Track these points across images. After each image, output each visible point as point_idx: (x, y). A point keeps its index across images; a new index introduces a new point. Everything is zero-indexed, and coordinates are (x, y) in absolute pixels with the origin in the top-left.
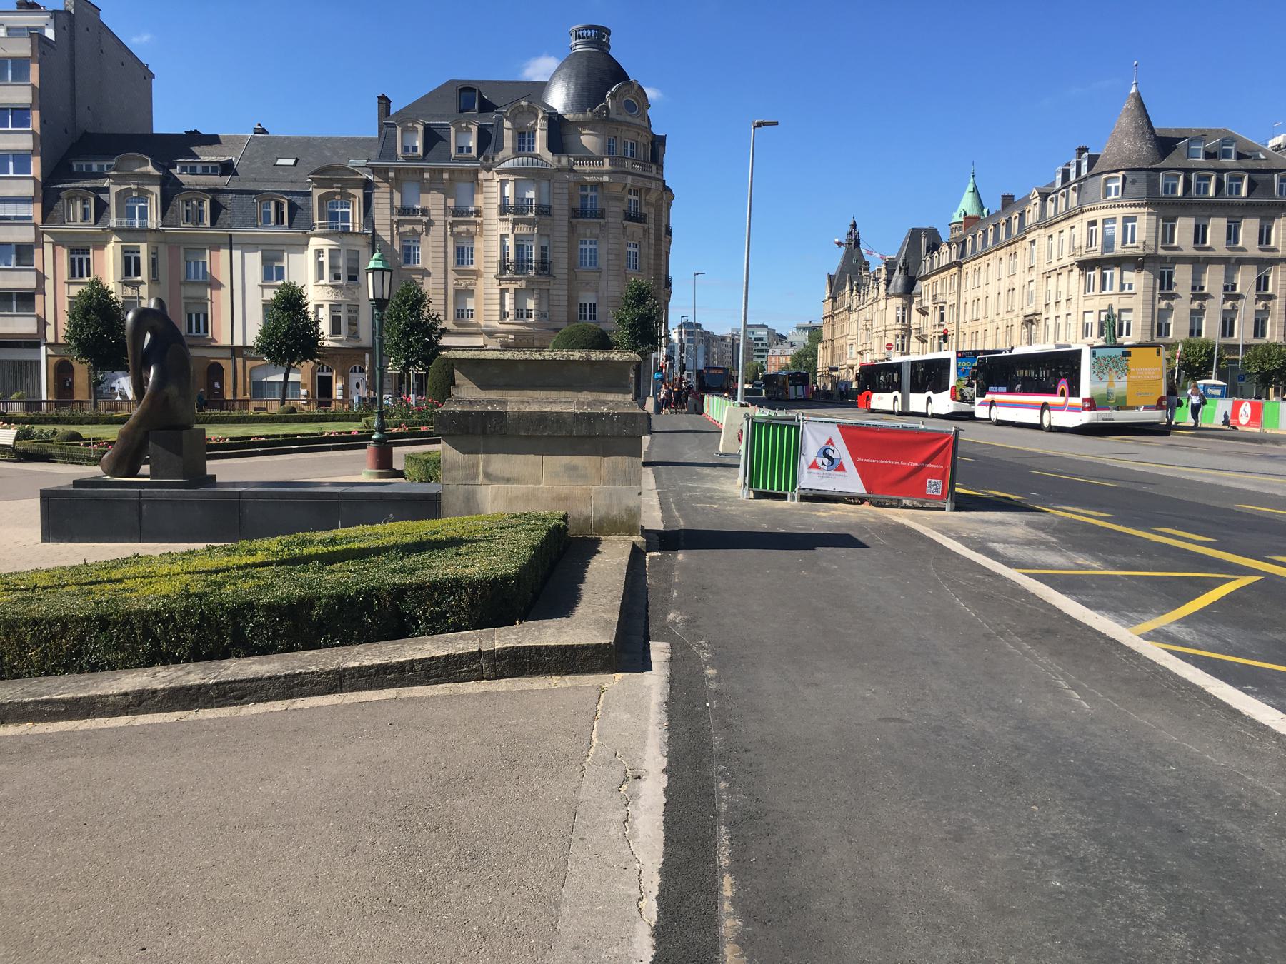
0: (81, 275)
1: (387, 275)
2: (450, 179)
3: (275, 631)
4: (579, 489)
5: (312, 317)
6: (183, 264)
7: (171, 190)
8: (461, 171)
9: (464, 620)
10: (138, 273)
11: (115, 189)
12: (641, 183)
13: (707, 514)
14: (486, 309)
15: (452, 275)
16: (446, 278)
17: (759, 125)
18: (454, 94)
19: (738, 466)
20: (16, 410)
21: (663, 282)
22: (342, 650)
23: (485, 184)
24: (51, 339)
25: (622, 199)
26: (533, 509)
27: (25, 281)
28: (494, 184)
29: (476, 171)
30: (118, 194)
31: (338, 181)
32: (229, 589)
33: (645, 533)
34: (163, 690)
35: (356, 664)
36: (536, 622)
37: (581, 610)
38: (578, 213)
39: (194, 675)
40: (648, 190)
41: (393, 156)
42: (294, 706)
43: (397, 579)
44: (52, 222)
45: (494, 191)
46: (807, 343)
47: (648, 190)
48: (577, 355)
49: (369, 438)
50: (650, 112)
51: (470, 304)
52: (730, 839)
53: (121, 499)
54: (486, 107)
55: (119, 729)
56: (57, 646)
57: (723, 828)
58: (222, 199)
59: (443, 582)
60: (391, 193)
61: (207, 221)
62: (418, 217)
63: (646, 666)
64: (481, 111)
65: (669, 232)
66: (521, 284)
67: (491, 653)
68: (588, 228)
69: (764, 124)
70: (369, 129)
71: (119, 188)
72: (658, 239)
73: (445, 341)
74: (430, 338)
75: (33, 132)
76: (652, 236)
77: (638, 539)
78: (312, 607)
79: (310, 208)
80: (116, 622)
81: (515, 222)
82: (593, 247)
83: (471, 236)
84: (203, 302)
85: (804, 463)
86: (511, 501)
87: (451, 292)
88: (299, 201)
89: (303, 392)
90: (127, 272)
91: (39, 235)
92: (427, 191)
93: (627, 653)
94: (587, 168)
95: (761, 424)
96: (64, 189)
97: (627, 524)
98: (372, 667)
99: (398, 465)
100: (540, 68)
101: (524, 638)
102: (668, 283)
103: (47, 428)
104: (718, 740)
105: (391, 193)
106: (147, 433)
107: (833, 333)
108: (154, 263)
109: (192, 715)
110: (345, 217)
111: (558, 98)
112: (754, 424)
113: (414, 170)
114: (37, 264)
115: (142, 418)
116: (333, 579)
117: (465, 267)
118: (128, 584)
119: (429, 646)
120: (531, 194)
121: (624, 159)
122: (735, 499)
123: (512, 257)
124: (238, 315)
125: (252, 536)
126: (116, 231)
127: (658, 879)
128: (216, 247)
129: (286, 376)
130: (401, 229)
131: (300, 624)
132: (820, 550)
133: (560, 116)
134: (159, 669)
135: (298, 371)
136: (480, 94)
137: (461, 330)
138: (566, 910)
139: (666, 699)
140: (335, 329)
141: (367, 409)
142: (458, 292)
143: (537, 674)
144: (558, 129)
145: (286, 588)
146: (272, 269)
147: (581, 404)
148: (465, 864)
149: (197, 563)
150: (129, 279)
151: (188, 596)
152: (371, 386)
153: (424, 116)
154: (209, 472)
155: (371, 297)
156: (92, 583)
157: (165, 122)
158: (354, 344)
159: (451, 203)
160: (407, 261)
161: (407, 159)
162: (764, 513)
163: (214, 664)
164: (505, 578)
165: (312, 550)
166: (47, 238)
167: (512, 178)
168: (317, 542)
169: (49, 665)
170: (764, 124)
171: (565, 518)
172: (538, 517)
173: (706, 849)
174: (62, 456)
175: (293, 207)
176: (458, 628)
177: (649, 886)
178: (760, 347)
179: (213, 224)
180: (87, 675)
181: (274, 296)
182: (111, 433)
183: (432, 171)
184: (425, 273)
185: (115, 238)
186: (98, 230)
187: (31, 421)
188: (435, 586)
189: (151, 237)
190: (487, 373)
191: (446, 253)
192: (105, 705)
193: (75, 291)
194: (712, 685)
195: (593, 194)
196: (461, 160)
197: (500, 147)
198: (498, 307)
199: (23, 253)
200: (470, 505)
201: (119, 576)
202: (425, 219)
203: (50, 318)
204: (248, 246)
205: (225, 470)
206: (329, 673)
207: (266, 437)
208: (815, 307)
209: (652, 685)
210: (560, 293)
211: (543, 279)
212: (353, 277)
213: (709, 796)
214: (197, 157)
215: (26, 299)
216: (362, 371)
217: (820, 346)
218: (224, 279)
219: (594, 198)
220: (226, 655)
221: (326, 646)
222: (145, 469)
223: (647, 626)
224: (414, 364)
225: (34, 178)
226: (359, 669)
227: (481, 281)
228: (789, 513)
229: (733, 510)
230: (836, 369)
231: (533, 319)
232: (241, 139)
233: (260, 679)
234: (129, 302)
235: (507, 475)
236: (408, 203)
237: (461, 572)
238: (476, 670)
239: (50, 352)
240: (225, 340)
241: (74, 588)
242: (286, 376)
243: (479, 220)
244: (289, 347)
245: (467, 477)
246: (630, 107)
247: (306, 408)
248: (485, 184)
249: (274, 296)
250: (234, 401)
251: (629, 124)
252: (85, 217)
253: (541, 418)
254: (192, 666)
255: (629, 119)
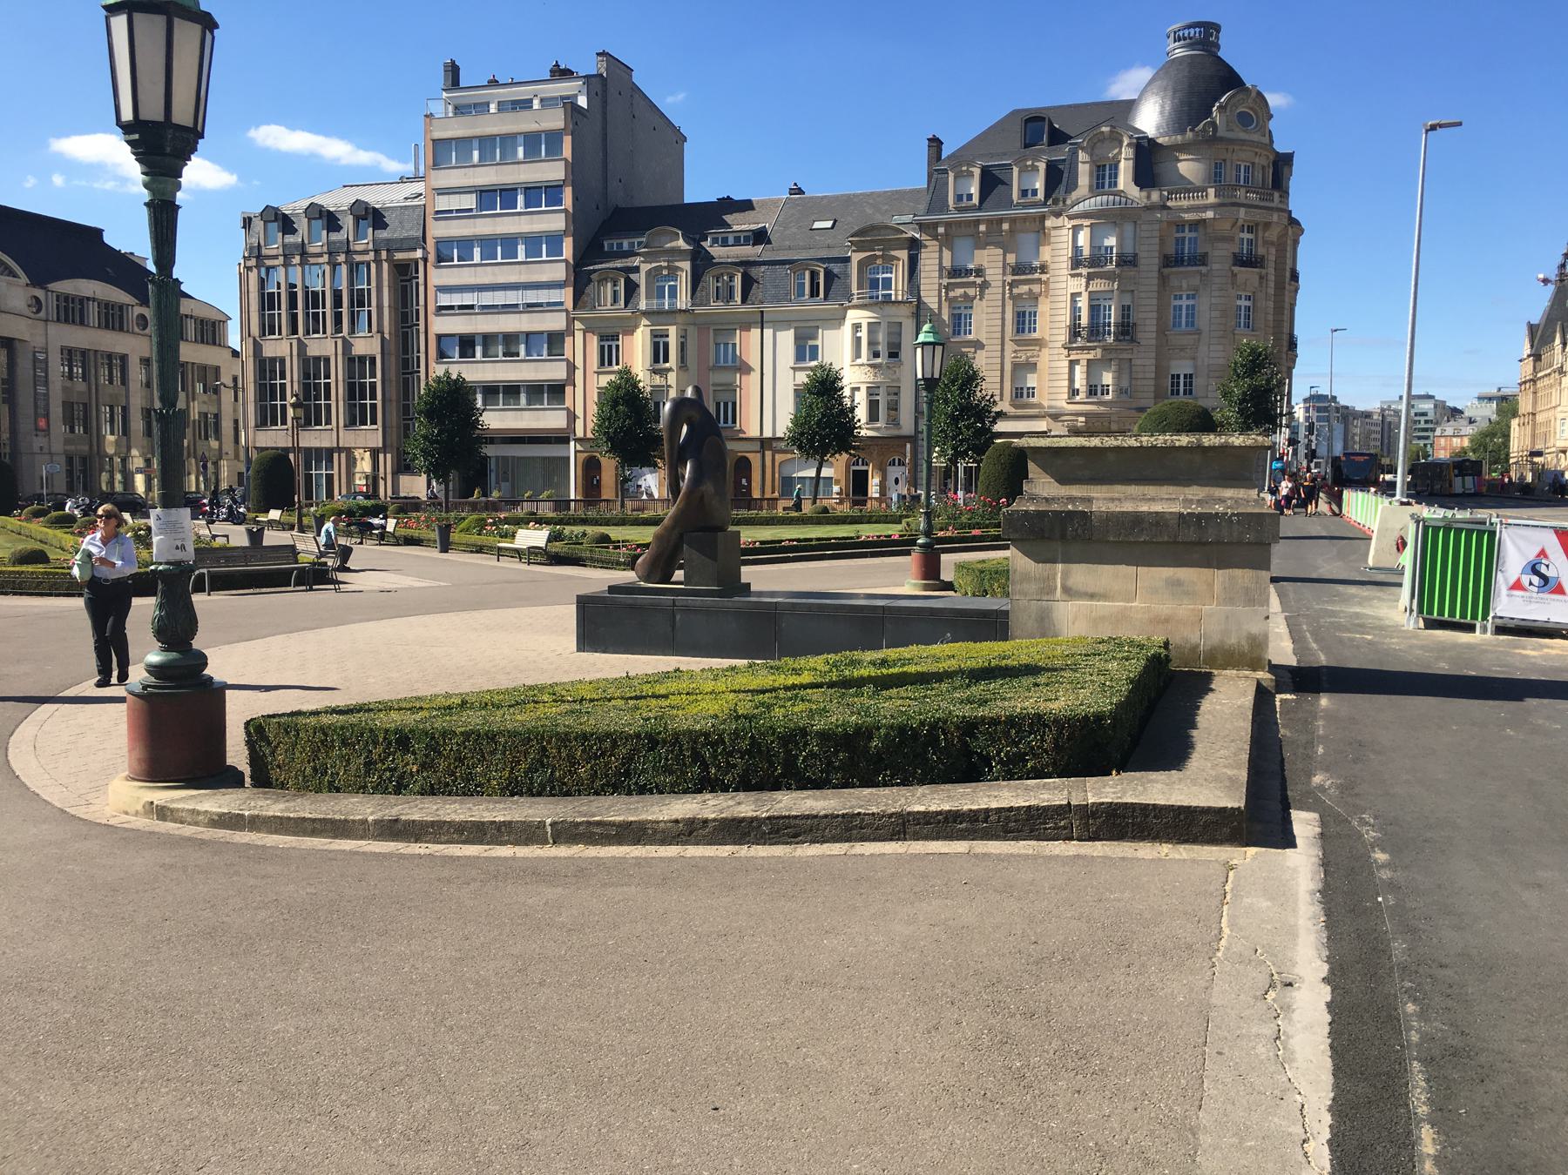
0: (610, 364)
1: (939, 349)
2: (1011, 230)
3: (830, 764)
4: (1184, 609)
5: (847, 402)
6: (712, 346)
7: (701, 263)
8: (1025, 219)
9: (1047, 766)
10: (666, 360)
11: (645, 268)
12: (1258, 216)
13: (1358, 647)
14: (1051, 386)
15: (1010, 347)
16: (1003, 350)
17: (1433, 128)
18: (1018, 128)
19: (1400, 585)
20: (546, 510)
21: (1285, 344)
22: (904, 790)
23: (1053, 233)
24: (580, 434)
25: (1230, 239)
26: (1125, 633)
27: (556, 372)
28: (1065, 232)
29: (1043, 218)
30: (649, 273)
31: (878, 242)
32: (778, 712)
33: (1274, 668)
34: (714, 820)
35: (922, 809)
36: (1138, 774)
37: (1196, 761)
38: (1171, 261)
39: (745, 806)
40: (1267, 225)
41: (944, 207)
42: (853, 852)
43: (967, 711)
44: (583, 308)
45: (1065, 239)
46: (1494, 417)
47: (1267, 225)
48: (1184, 440)
49: (913, 542)
50: (1272, 125)
51: (1032, 381)
52: (1427, 1081)
53: (656, 608)
54: (1058, 138)
55: (671, 859)
56: (606, 764)
57: (1415, 1064)
58: (754, 272)
59: (1022, 717)
60: (941, 251)
61: (738, 298)
62: (972, 279)
63: (1286, 840)
64: (1051, 144)
65: (1295, 277)
66: (1096, 354)
67: (1083, 808)
68: (1184, 278)
69: (1441, 126)
70: (916, 178)
71: (649, 266)
72: (1280, 287)
73: (1001, 426)
74: (983, 423)
75: (566, 211)
76: (1272, 285)
77: (1264, 675)
78: (870, 738)
79: (847, 276)
80: (665, 742)
81: (1090, 278)
82: (1191, 302)
83: (1035, 298)
84: (731, 389)
85: (1502, 582)
86: (1096, 621)
87: (1008, 367)
88: (836, 268)
89: (836, 489)
90: (656, 360)
91: (570, 321)
92: (981, 245)
93: (1261, 820)
94: (1185, 203)
95: (1436, 529)
96: (595, 271)
97: (1249, 656)
98: (940, 813)
99: (947, 575)
100: (1123, 87)
101: (1124, 792)
102: (1293, 345)
103: (578, 529)
104: (1398, 947)
105: (941, 251)
106: (681, 536)
107: (1535, 403)
108: (682, 347)
109: (744, 851)
110: (887, 284)
111: (1150, 119)
112: (1426, 528)
113: (968, 223)
114: (568, 353)
115: (677, 519)
116: (892, 707)
117: (1027, 336)
118: (673, 700)
119: (1006, 793)
120: (1111, 241)
121: (1235, 187)
122: (1396, 630)
123: (1084, 321)
124: (768, 405)
125: (796, 653)
126: (646, 314)
127: (1328, 1119)
128: (746, 327)
129: (819, 471)
130: (951, 294)
131: (858, 757)
132: (1532, 702)
133: (1152, 141)
134: (708, 796)
135: (831, 465)
136: (1051, 124)
137: (1020, 412)
138: (1205, 1140)
139: (1320, 886)
140: (873, 416)
141: (909, 509)
142: (1016, 367)
143: (1142, 839)
144: (1149, 157)
145: (840, 714)
146: (805, 349)
147: (1187, 502)
148: (1071, 1065)
149: (742, 681)
150: (658, 366)
151: (738, 717)
152: (913, 482)
153: (981, 157)
154: (744, 580)
155: (920, 376)
156: (637, 698)
157: (698, 189)
158: (895, 432)
159: (1011, 258)
160: (956, 332)
161: (959, 210)
162: (1442, 648)
163: (766, 795)
164: (1099, 717)
165: (864, 672)
166: (578, 325)
167: (1087, 222)
168: (867, 662)
169: (598, 784)
170: (1441, 126)
171: (1166, 645)
172: (1132, 643)
173: (1392, 1088)
174: (592, 560)
175: (830, 276)
176: (1039, 774)
177: (1315, 1125)
178: (1422, 425)
179: (744, 301)
180: (635, 798)
181: (806, 380)
182: (647, 534)
183: (989, 222)
184: (978, 345)
185: (645, 321)
186: (627, 313)
187: (560, 522)
188: (1011, 721)
189: (680, 318)
190: (1069, 465)
191: (1003, 319)
192: (655, 831)
193: (604, 380)
194: (1385, 874)
195: (1193, 235)
196: (1025, 206)
197: (1073, 185)
198: (1066, 383)
199: (555, 341)
200: (1044, 626)
201: (663, 692)
202: (979, 280)
203: (579, 412)
204: (780, 324)
205: (762, 579)
206: (891, 816)
207: (798, 540)
208: (1506, 366)
209: (1300, 864)
210: (1145, 362)
211: (1124, 345)
212: (894, 355)
213: (1391, 1021)
214: (729, 226)
215: (556, 391)
216: (901, 463)
217: (1514, 423)
218: (754, 362)
219: (1193, 241)
220: (776, 787)
221: (885, 785)
222: (679, 575)
223: (1284, 788)
224: (964, 454)
225: (566, 261)
226: (925, 814)
227: (1045, 351)
228: (1478, 648)
229: (1395, 643)
230: (1539, 454)
231: (1109, 397)
232: (775, 202)
233: (816, 817)
234: (660, 391)
235: (1090, 591)
236: (959, 263)
237: (1044, 707)
238: (1065, 828)
239: (579, 448)
240: (753, 432)
241: (620, 703)
242: (819, 471)
243: (1044, 277)
244: (823, 438)
245: (1042, 591)
246: (1245, 120)
247: (840, 508)
248: (1053, 233)
249: (806, 380)
250: (762, 499)
251: (1243, 142)
252: (615, 301)
253: (1137, 520)
254: (741, 795)
255: (1243, 136)
